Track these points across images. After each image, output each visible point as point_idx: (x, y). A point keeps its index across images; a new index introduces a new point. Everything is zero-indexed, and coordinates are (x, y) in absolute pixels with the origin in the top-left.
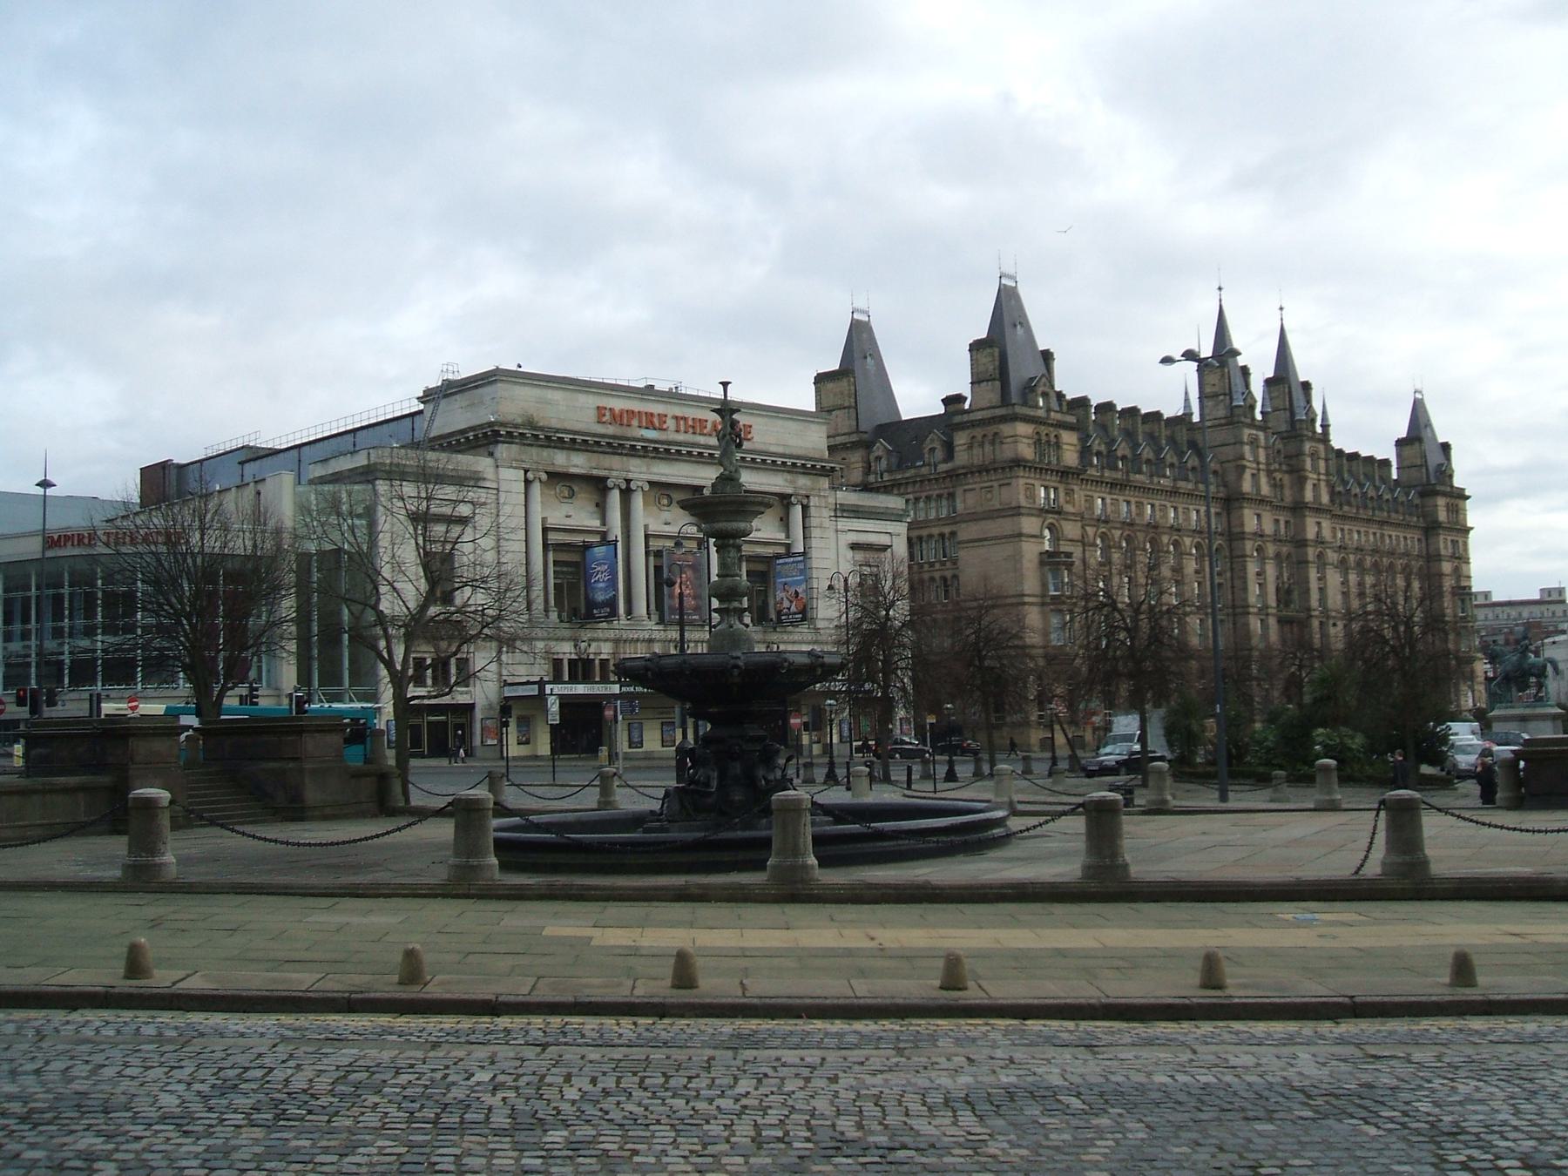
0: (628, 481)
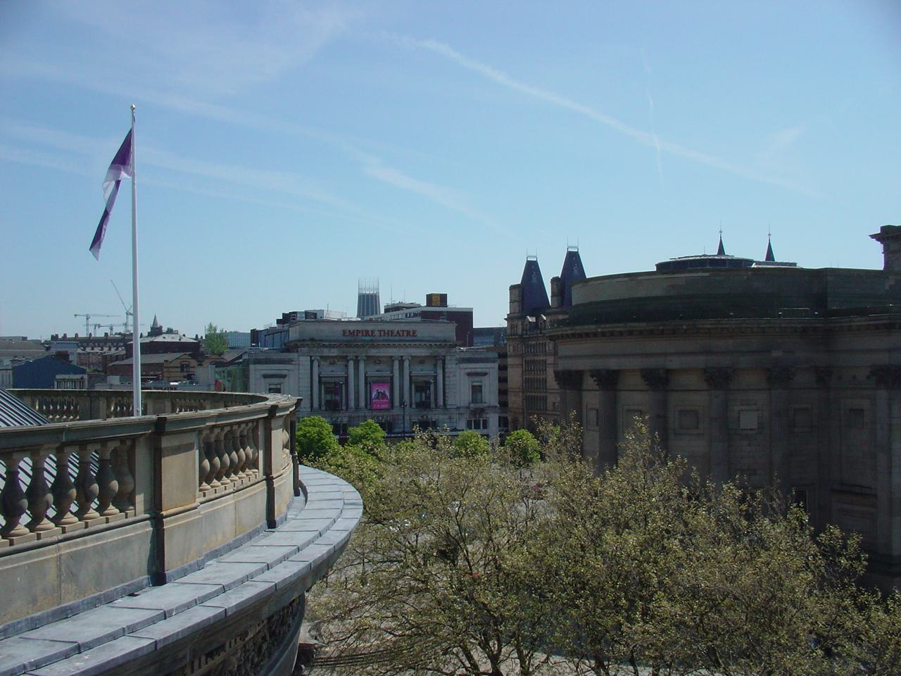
0: (357, 357)
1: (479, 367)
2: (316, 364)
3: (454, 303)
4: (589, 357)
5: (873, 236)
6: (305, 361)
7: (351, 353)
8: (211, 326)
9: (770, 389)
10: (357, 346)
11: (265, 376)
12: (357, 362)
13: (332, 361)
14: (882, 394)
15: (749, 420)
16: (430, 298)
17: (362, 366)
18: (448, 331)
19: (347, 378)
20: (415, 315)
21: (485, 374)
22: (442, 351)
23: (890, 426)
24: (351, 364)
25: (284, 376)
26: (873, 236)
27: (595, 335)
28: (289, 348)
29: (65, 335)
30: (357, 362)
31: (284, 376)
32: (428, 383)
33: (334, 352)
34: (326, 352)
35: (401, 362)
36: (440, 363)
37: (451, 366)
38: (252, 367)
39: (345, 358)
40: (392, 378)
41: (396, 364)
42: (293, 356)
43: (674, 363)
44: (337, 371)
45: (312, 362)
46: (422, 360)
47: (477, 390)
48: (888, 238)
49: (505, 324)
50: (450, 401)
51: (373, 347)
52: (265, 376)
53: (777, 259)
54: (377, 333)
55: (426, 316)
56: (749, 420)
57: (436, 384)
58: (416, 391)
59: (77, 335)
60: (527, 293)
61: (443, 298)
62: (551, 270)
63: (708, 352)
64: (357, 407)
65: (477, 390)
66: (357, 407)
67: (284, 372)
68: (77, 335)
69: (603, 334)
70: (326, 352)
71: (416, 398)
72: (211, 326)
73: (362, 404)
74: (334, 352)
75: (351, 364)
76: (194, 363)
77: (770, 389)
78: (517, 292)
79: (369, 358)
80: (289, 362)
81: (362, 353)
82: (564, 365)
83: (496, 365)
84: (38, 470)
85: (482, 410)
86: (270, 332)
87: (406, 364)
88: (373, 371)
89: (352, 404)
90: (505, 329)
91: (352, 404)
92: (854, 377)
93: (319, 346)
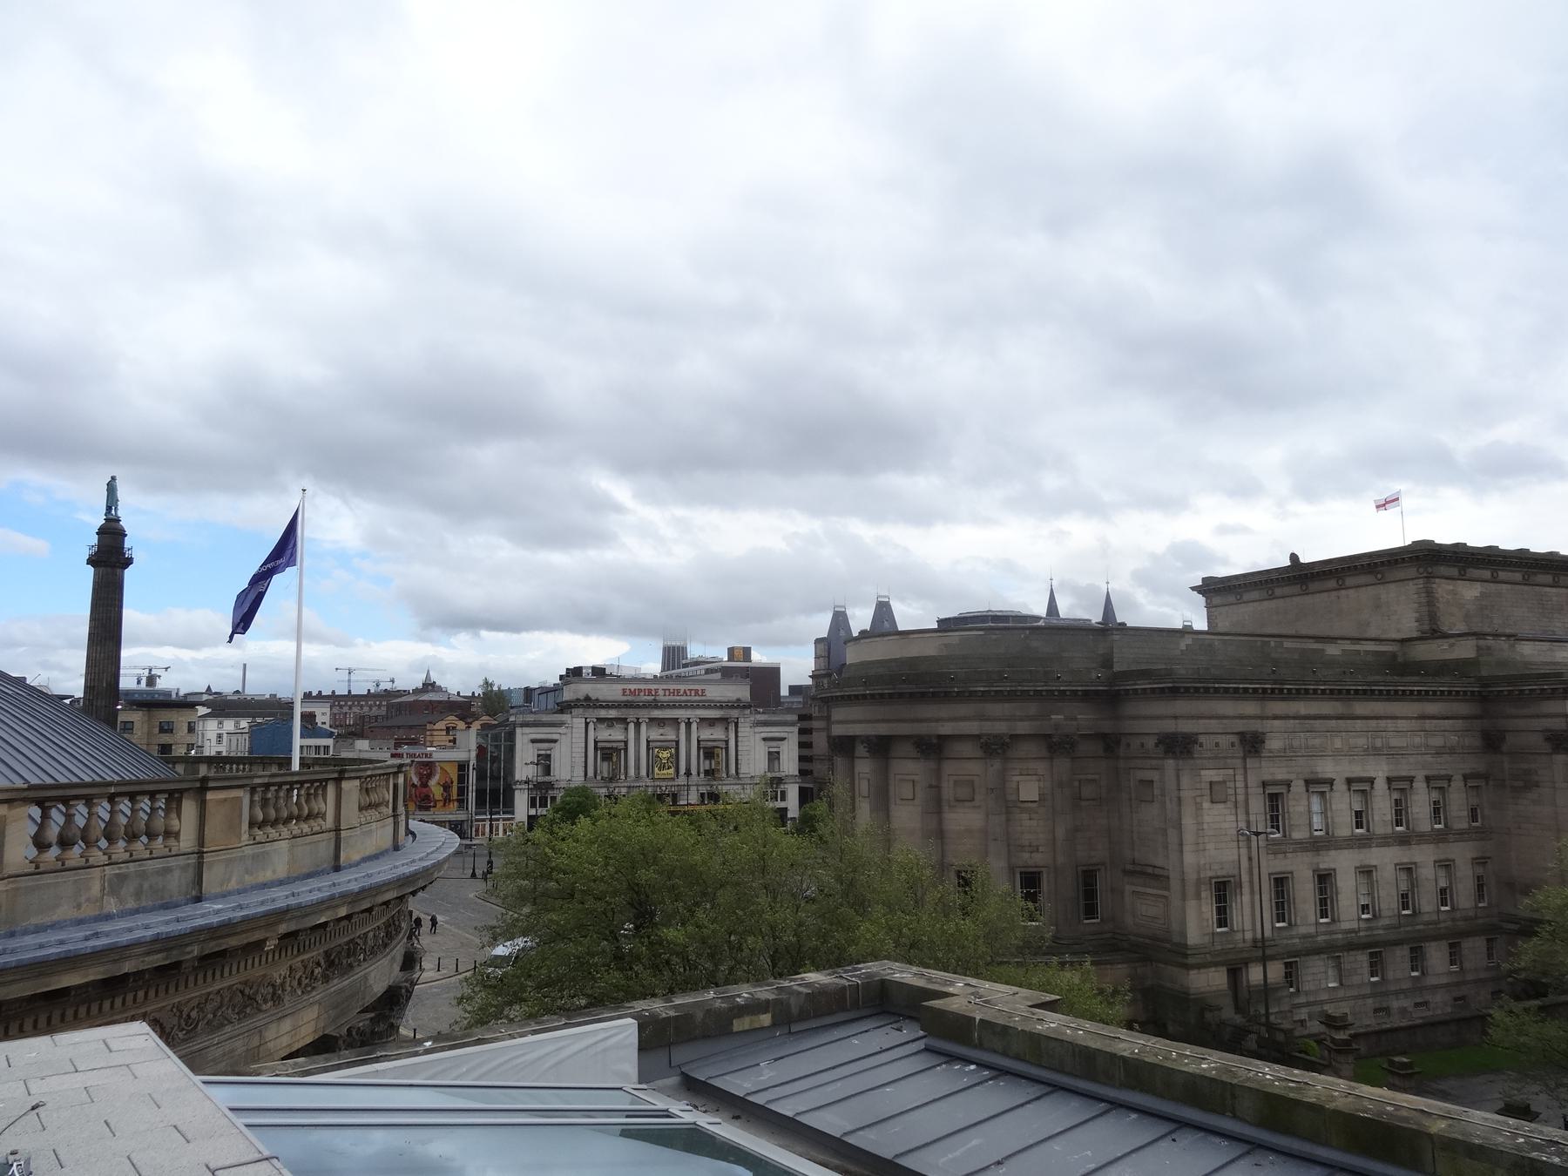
1: (775, 731)
2: (591, 726)
3: (759, 657)
4: (860, 722)
5: (1193, 589)
6: (579, 723)
7: (631, 714)
8: (486, 682)
9: (1051, 758)
10: (638, 707)
11: (533, 741)
12: (638, 725)
13: (610, 722)
14: (1170, 763)
15: (1029, 790)
16: (731, 651)
17: (643, 728)
18: (742, 692)
19: (626, 743)
20: (708, 671)
21: (783, 739)
22: (734, 713)
23: (1179, 799)
24: (632, 726)
25: (555, 741)
26: (1193, 589)
27: (864, 697)
28: (565, 707)
29: (883, 611)
30: (638, 725)
31: (555, 741)
32: (618, 750)
33: (613, 713)
34: (603, 713)
35: (688, 724)
36: (732, 727)
37: (745, 730)
38: (518, 730)
39: (624, 721)
40: (677, 742)
41: (683, 726)
42: (566, 717)
43: (946, 729)
44: (616, 734)
45: (587, 724)
46: (711, 722)
47: (774, 757)
48: (1210, 591)
49: (809, 682)
50: (743, 769)
51: (656, 707)
52: (533, 741)
53: (1062, 614)
54: (661, 692)
55: (727, 673)
56: (1029, 790)
57: (727, 749)
58: (603, 759)
59: (1294, 557)
60: (830, 648)
61: (747, 652)
62: (861, 619)
63: (982, 718)
64: (638, 776)
65: (774, 757)
66: (638, 776)
67: (555, 737)
68: (1294, 557)
69: (872, 696)
70: (603, 713)
71: (705, 765)
72: (486, 682)
73: (643, 772)
74: (613, 713)
75: (632, 726)
76: (461, 725)
77: (1051, 758)
78: (821, 646)
79: (600, 720)
80: (560, 724)
81: (644, 714)
82: (838, 730)
83: (796, 729)
84: (69, 818)
85: (780, 780)
86: (545, 691)
87: (694, 726)
88: (655, 734)
89: (632, 772)
90: (808, 687)
91: (632, 772)
92: (1217, 745)
93: (595, 707)
